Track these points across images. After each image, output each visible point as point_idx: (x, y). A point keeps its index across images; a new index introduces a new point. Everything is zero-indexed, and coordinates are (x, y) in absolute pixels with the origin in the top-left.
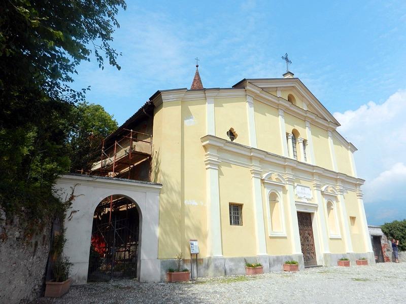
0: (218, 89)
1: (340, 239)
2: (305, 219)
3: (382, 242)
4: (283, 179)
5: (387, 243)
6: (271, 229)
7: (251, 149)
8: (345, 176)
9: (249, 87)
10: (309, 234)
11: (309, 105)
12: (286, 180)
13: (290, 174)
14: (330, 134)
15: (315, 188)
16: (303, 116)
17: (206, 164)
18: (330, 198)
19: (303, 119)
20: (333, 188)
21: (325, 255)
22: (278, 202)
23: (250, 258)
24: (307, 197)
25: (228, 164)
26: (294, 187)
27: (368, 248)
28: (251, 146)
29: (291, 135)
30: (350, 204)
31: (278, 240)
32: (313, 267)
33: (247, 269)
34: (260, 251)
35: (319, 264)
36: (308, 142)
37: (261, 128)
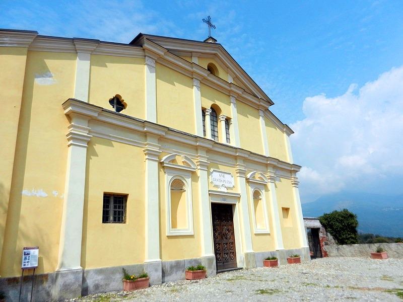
0: (98, 42)
1: (269, 234)
2: (222, 214)
3: (321, 235)
4: (264, 176)
5: (325, 236)
6: (168, 224)
7: (144, 123)
8: (277, 161)
9: (146, 45)
10: (228, 230)
11: (236, 78)
12: (196, 164)
13: (242, 166)
14: (261, 113)
15: (238, 175)
16: (256, 104)
17: (69, 140)
18: (257, 186)
19: (228, 93)
20: (262, 174)
21: (247, 255)
22: (185, 191)
23: (134, 267)
24: (227, 185)
25: (108, 141)
26: (209, 174)
27: (302, 243)
28: (146, 118)
29: (208, 113)
30: (280, 194)
31: (181, 240)
32: (229, 271)
33: (125, 283)
34: (149, 255)
35: (239, 266)
36: (232, 121)
37: (173, 103)
